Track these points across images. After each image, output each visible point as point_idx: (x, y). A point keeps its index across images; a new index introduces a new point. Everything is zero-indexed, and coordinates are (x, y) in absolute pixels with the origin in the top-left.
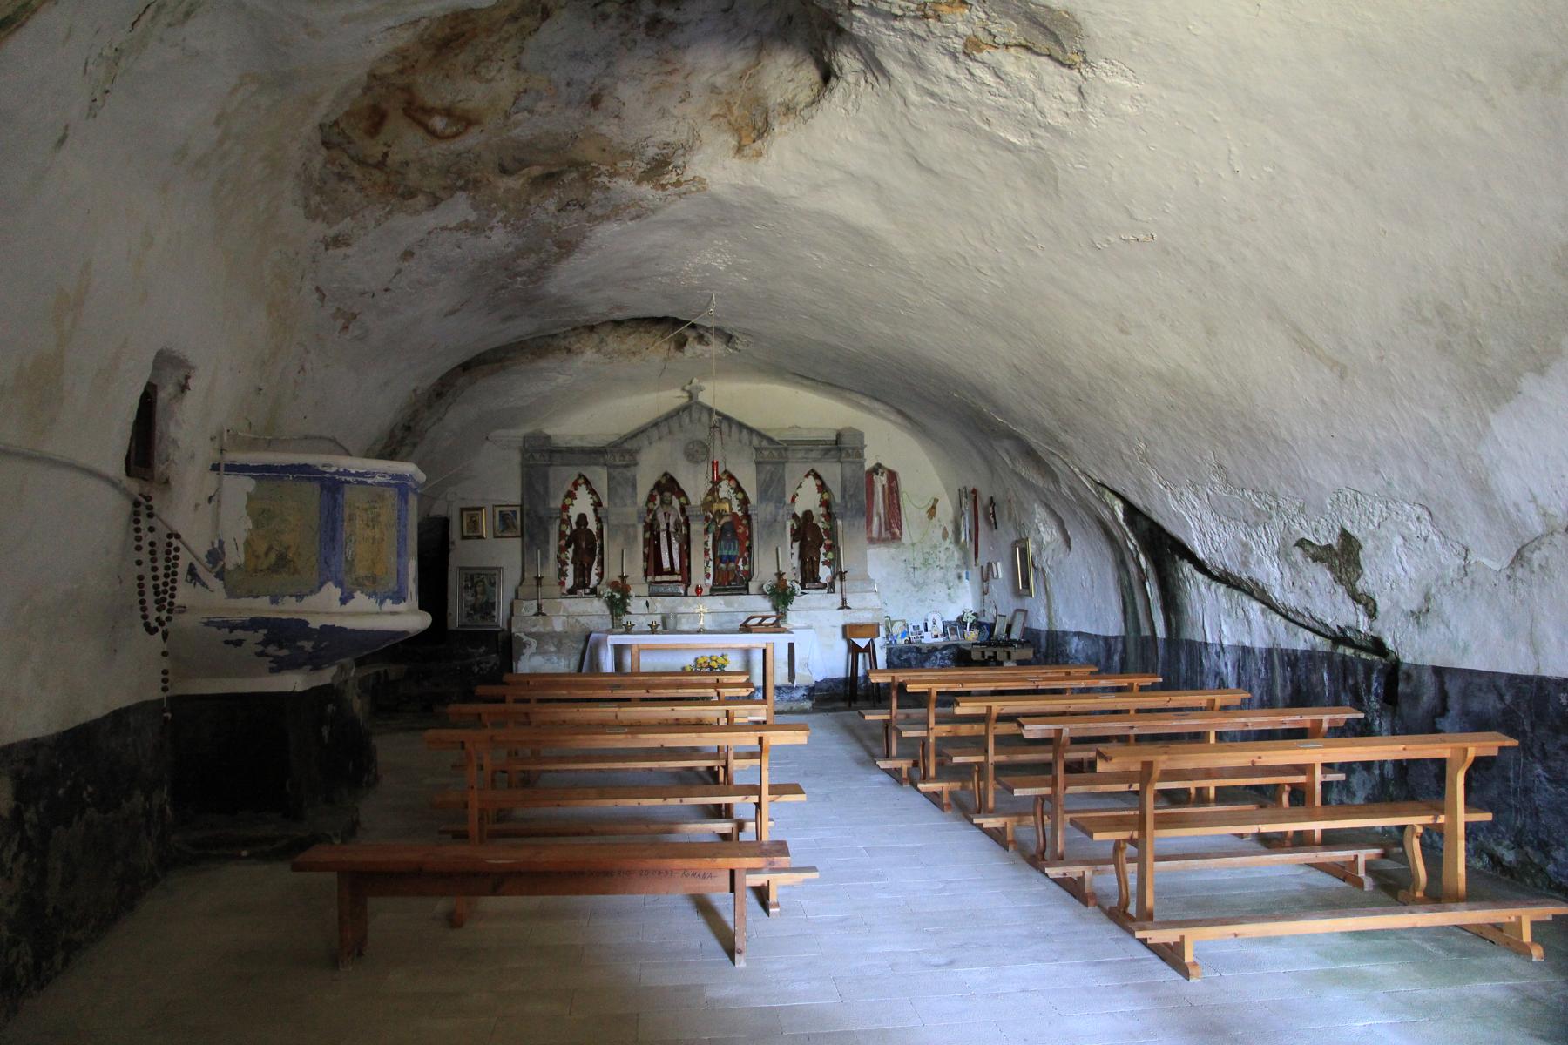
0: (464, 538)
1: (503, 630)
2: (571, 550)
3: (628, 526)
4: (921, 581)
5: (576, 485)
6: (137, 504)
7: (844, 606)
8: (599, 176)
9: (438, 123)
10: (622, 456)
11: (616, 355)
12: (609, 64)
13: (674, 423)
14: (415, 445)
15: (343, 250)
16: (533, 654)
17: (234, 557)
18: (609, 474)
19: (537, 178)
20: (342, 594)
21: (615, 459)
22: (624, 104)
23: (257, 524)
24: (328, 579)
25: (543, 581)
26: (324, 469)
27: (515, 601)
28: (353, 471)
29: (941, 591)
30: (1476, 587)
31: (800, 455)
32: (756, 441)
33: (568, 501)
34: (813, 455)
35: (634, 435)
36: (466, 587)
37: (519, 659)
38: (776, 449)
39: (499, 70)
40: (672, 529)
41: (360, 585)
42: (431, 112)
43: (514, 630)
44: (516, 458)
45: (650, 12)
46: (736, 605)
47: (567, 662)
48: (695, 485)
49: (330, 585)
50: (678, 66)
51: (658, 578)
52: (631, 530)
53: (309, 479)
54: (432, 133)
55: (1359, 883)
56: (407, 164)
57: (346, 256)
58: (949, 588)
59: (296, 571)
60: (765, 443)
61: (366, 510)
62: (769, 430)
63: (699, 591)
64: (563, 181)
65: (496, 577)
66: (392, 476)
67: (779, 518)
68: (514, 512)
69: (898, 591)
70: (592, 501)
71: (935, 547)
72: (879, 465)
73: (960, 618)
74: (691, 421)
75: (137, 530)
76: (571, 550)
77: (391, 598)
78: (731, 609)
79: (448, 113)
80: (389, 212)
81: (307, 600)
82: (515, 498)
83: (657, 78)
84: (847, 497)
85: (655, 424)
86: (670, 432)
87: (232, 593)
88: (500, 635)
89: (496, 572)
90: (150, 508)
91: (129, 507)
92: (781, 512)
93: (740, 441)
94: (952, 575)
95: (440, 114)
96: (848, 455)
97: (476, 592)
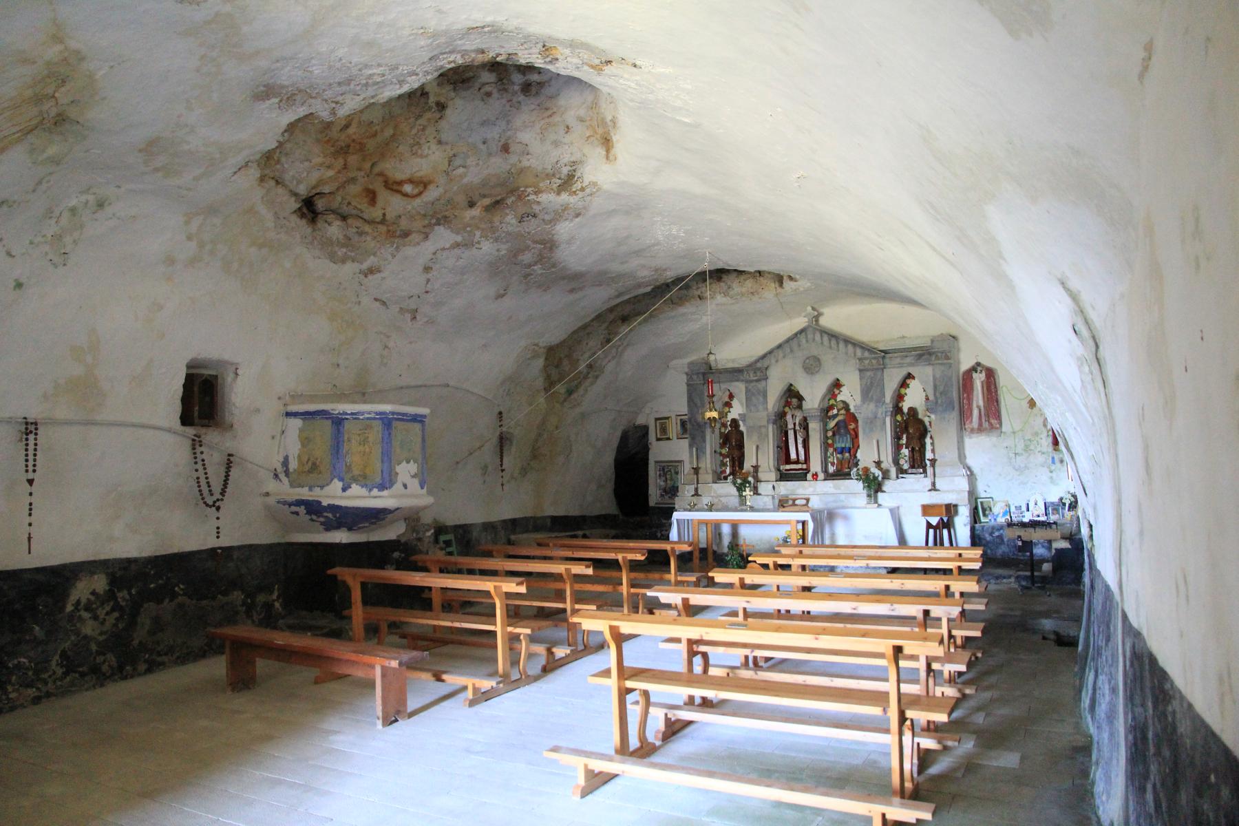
0: (658, 440)
3: (760, 427)
4: (1022, 465)
6: (194, 440)
8: (528, 195)
9: (408, 188)
11: (739, 297)
12: (508, 122)
13: (794, 343)
14: (597, 377)
15: (378, 276)
17: (293, 465)
18: (746, 388)
19: (488, 206)
20: (343, 485)
21: (749, 376)
22: (527, 145)
23: (303, 445)
24: (335, 477)
26: (332, 412)
28: (349, 412)
29: (1043, 474)
31: (898, 360)
32: (859, 352)
34: (908, 360)
35: (764, 357)
38: (875, 358)
39: (429, 148)
41: (355, 480)
42: (401, 183)
45: (520, 82)
46: (842, 488)
48: (813, 394)
49: (336, 480)
50: (555, 110)
53: (327, 418)
54: (406, 195)
56: (400, 217)
57: (383, 278)
59: (320, 473)
60: (867, 354)
61: (359, 435)
62: (878, 342)
63: (815, 476)
64: (507, 204)
66: (377, 413)
67: (879, 415)
69: (1000, 475)
71: (1036, 434)
72: (978, 364)
73: (1061, 499)
74: (807, 341)
75: (195, 453)
77: (377, 488)
78: (839, 492)
79: (410, 181)
80: (397, 248)
81: (326, 488)
82: (684, 409)
83: (543, 122)
84: (938, 394)
85: (779, 346)
86: (792, 351)
87: (292, 486)
90: (200, 441)
91: (190, 442)
93: (847, 353)
95: (407, 183)
96: (937, 358)
97: (666, 479)
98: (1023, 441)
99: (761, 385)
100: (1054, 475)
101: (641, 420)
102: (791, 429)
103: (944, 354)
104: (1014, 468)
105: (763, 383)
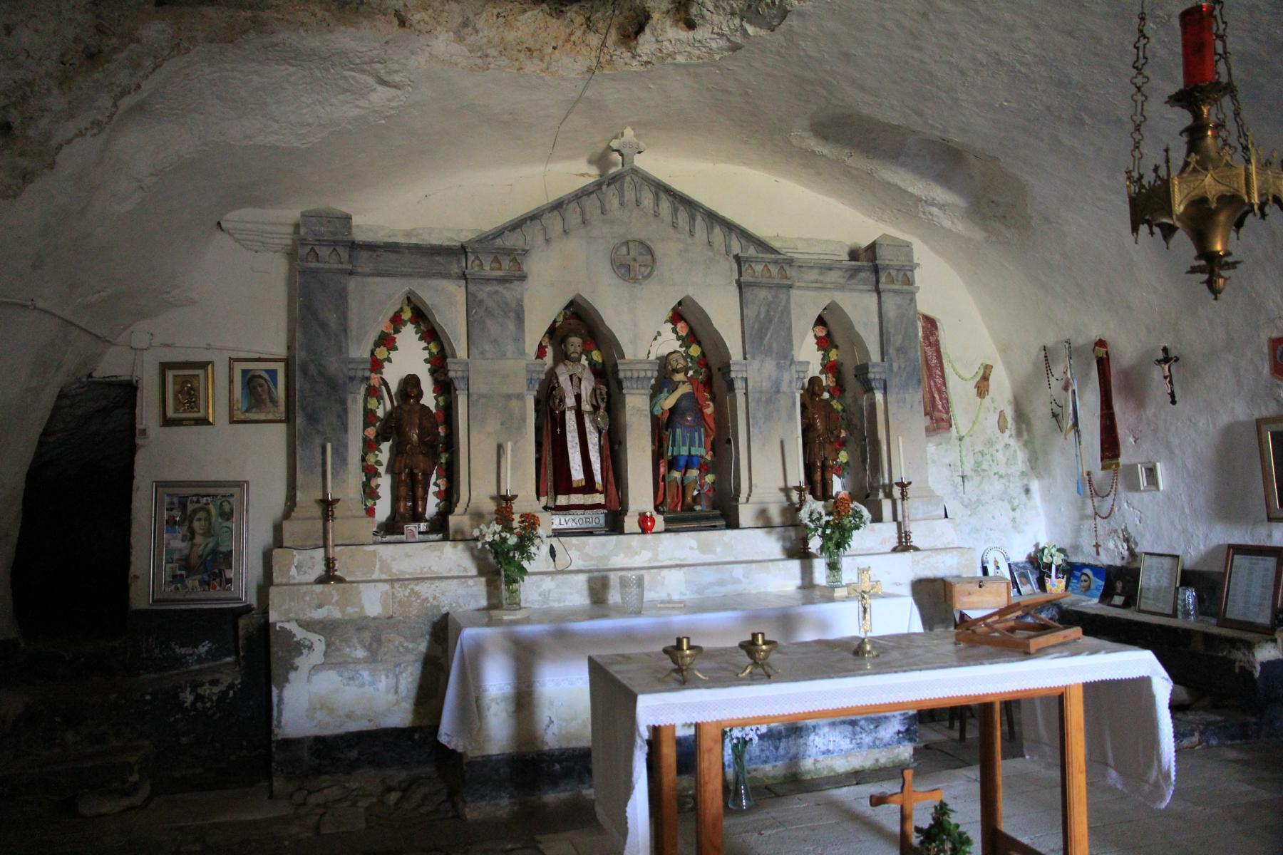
0: (167, 422)
1: (248, 609)
2: (386, 447)
3: (508, 397)
5: (397, 321)
7: (904, 545)
10: (496, 260)
16: (316, 668)
25: (338, 510)
27: (277, 552)
30: (490, 507)
32: (736, 248)
33: (381, 353)
35: (517, 225)
36: (171, 523)
37: (287, 680)
38: (776, 262)
40: (586, 407)
43: (273, 616)
44: (277, 268)
46: (719, 550)
47: (392, 681)
51: (562, 500)
52: (514, 404)
55: (307, 625)
58: (1014, 510)
60: (752, 251)
65: (234, 501)
67: (784, 387)
68: (272, 373)
70: (426, 355)
76: (386, 447)
82: (275, 344)
86: (584, 222)
88: (242, 622)
89: (236, 491)
92: (786, 376)
94: (1016, 487)
97: (193, 533)
98: (971, 454)
99: (509, 293)
100: (1017, 514)
101: (113, 365)
102: (570, 409)
103: (901, 273)
104: (962, 503)
105: (516, 286)
